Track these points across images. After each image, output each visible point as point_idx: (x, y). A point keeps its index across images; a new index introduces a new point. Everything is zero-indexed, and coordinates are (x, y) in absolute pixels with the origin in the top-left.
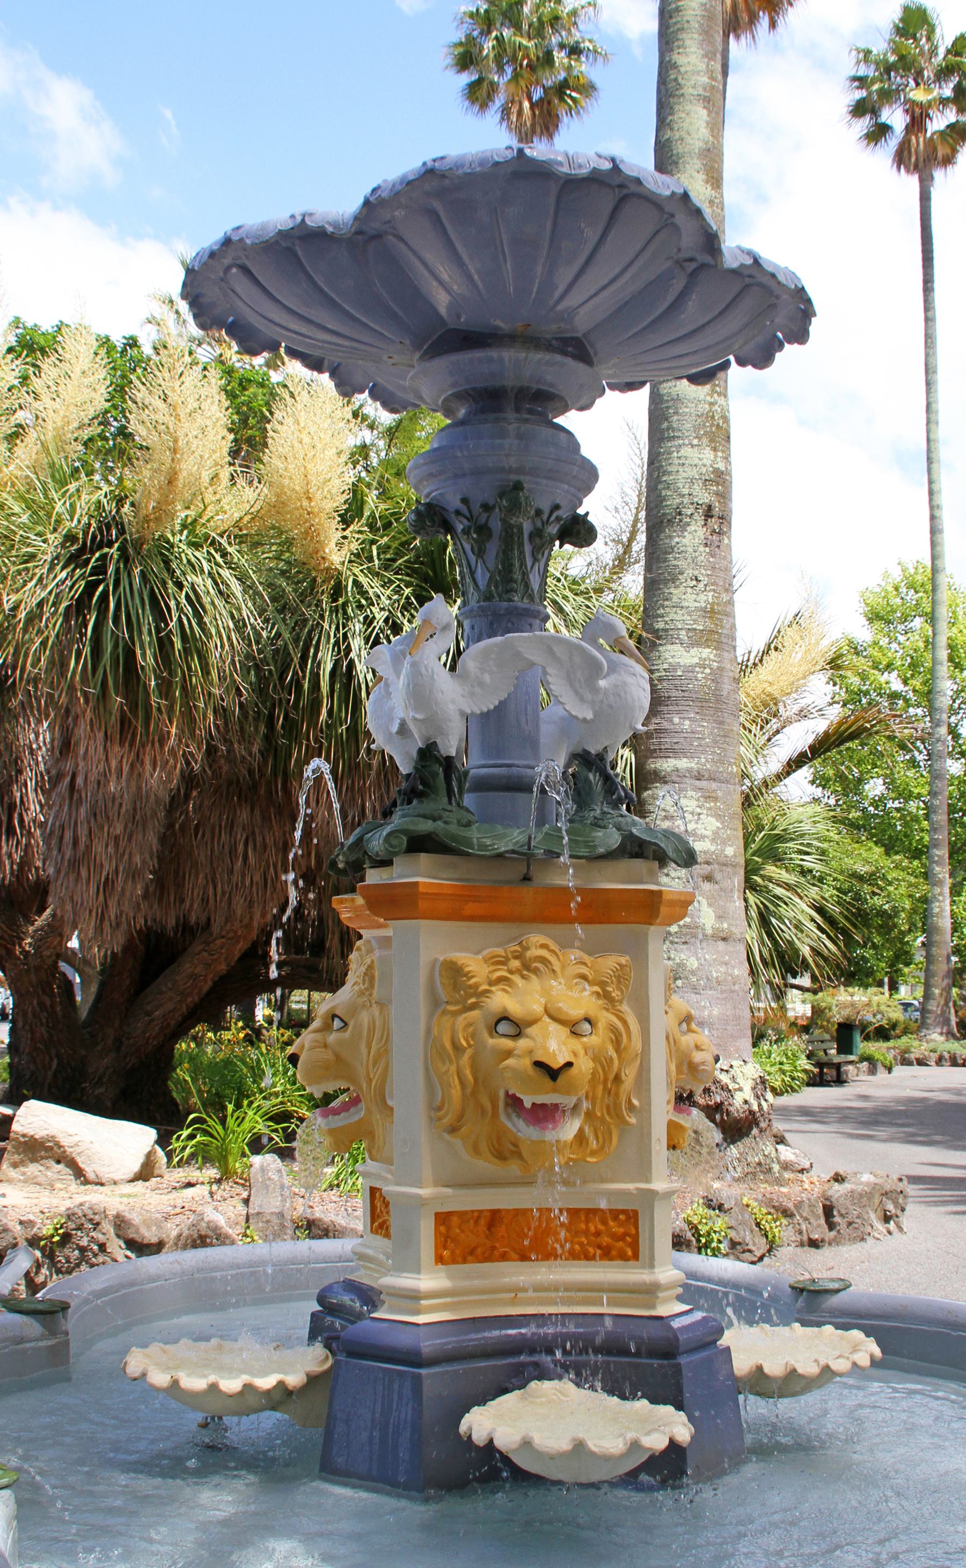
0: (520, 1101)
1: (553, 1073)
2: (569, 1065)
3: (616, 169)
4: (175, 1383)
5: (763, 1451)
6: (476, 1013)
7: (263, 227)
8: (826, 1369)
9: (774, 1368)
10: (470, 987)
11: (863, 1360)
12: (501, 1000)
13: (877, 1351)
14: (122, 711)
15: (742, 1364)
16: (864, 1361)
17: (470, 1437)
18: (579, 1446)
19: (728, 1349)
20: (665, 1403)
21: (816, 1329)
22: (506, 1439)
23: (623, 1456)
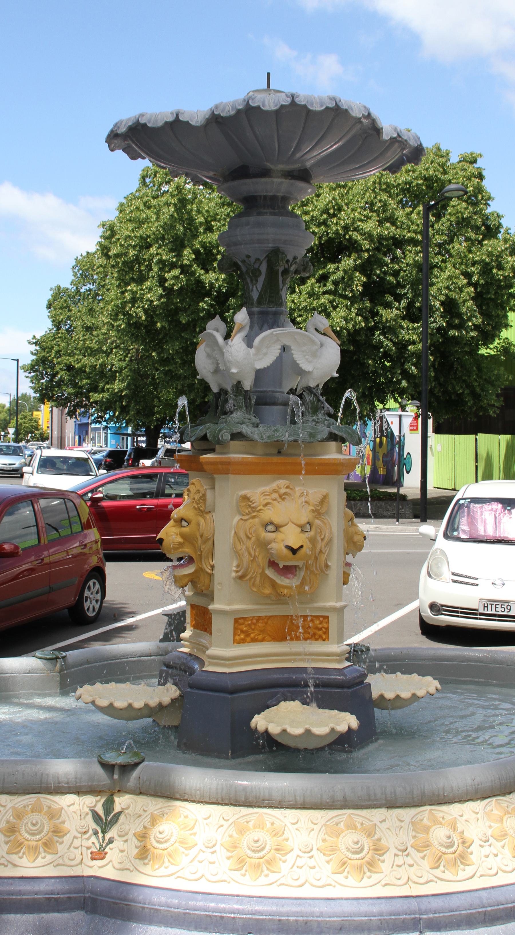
0: (277, 565)
1: (294, 551)
2: (302, 547)
3: (293, 103)
4: (111, 705)
5: (386, 734)
6: (256, 520)
7: (129, 120)
8: (414, 695)
9: (390, 695)
10: (253, 508)
11: (432, 690)
12: (268, 514)
13: (439, 686)
14: (284, 281)
15: (375, 694)
16: (432, 690)
17: (256, 728)
18: (308, 732)
19: (369, 685)
20: (345, 711)
21: (409, 676)
22: (274, 729)
23: (327, 735)
